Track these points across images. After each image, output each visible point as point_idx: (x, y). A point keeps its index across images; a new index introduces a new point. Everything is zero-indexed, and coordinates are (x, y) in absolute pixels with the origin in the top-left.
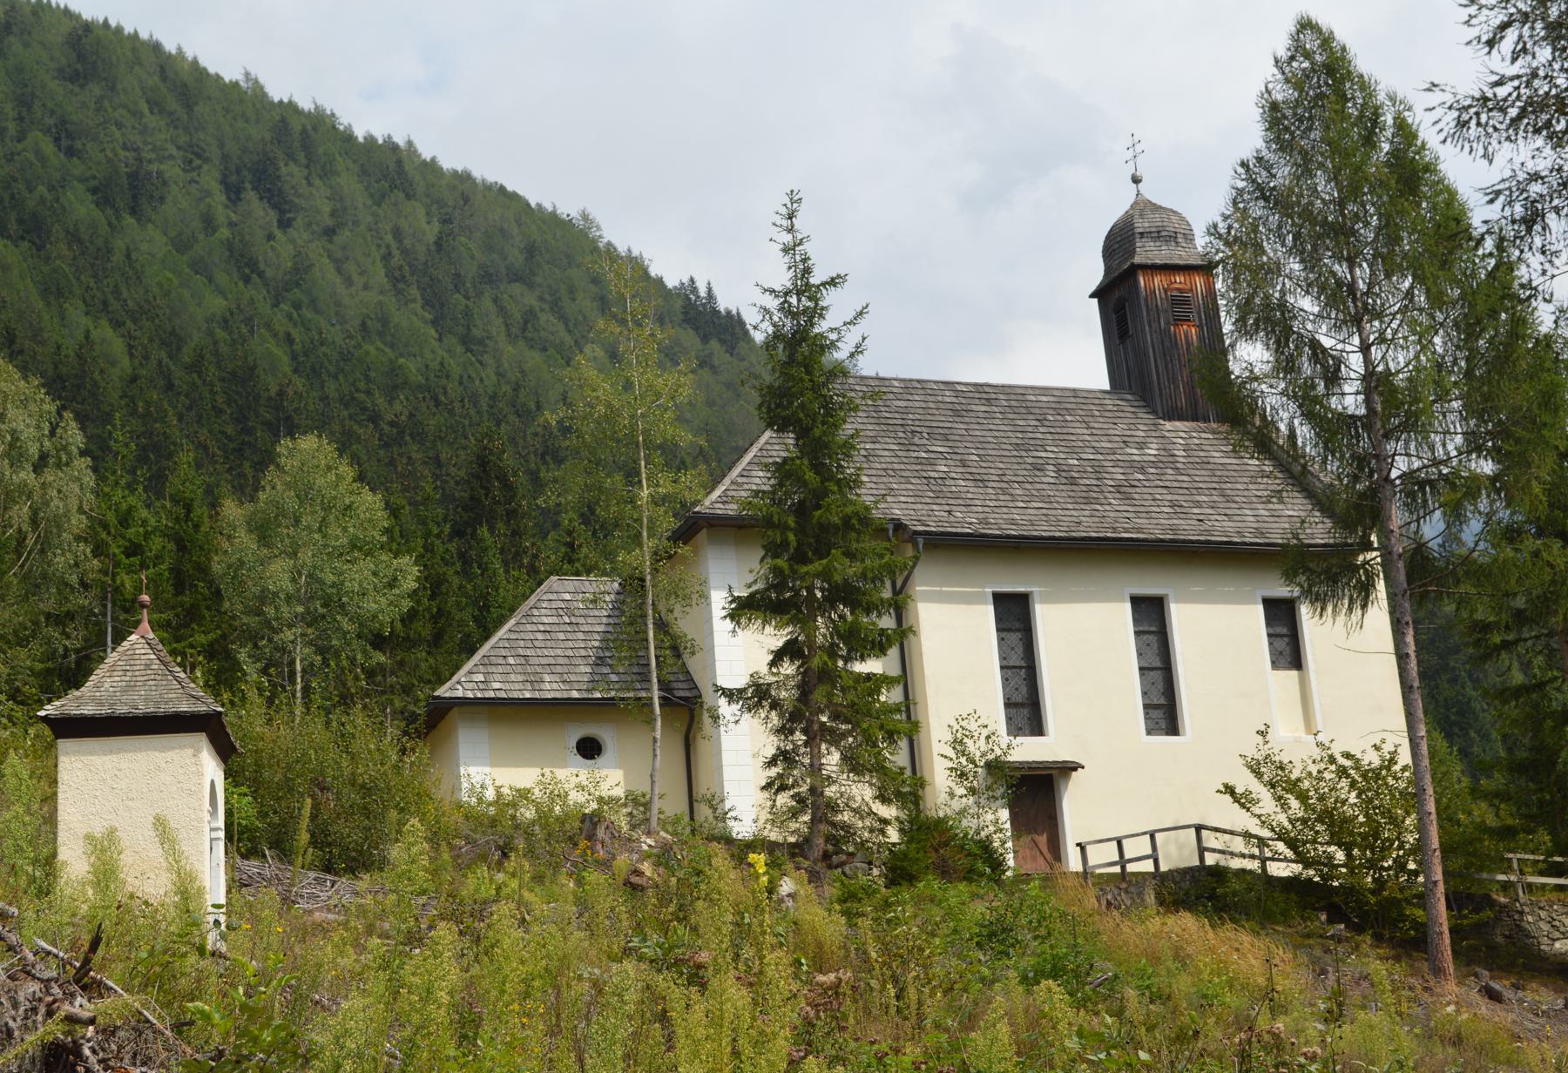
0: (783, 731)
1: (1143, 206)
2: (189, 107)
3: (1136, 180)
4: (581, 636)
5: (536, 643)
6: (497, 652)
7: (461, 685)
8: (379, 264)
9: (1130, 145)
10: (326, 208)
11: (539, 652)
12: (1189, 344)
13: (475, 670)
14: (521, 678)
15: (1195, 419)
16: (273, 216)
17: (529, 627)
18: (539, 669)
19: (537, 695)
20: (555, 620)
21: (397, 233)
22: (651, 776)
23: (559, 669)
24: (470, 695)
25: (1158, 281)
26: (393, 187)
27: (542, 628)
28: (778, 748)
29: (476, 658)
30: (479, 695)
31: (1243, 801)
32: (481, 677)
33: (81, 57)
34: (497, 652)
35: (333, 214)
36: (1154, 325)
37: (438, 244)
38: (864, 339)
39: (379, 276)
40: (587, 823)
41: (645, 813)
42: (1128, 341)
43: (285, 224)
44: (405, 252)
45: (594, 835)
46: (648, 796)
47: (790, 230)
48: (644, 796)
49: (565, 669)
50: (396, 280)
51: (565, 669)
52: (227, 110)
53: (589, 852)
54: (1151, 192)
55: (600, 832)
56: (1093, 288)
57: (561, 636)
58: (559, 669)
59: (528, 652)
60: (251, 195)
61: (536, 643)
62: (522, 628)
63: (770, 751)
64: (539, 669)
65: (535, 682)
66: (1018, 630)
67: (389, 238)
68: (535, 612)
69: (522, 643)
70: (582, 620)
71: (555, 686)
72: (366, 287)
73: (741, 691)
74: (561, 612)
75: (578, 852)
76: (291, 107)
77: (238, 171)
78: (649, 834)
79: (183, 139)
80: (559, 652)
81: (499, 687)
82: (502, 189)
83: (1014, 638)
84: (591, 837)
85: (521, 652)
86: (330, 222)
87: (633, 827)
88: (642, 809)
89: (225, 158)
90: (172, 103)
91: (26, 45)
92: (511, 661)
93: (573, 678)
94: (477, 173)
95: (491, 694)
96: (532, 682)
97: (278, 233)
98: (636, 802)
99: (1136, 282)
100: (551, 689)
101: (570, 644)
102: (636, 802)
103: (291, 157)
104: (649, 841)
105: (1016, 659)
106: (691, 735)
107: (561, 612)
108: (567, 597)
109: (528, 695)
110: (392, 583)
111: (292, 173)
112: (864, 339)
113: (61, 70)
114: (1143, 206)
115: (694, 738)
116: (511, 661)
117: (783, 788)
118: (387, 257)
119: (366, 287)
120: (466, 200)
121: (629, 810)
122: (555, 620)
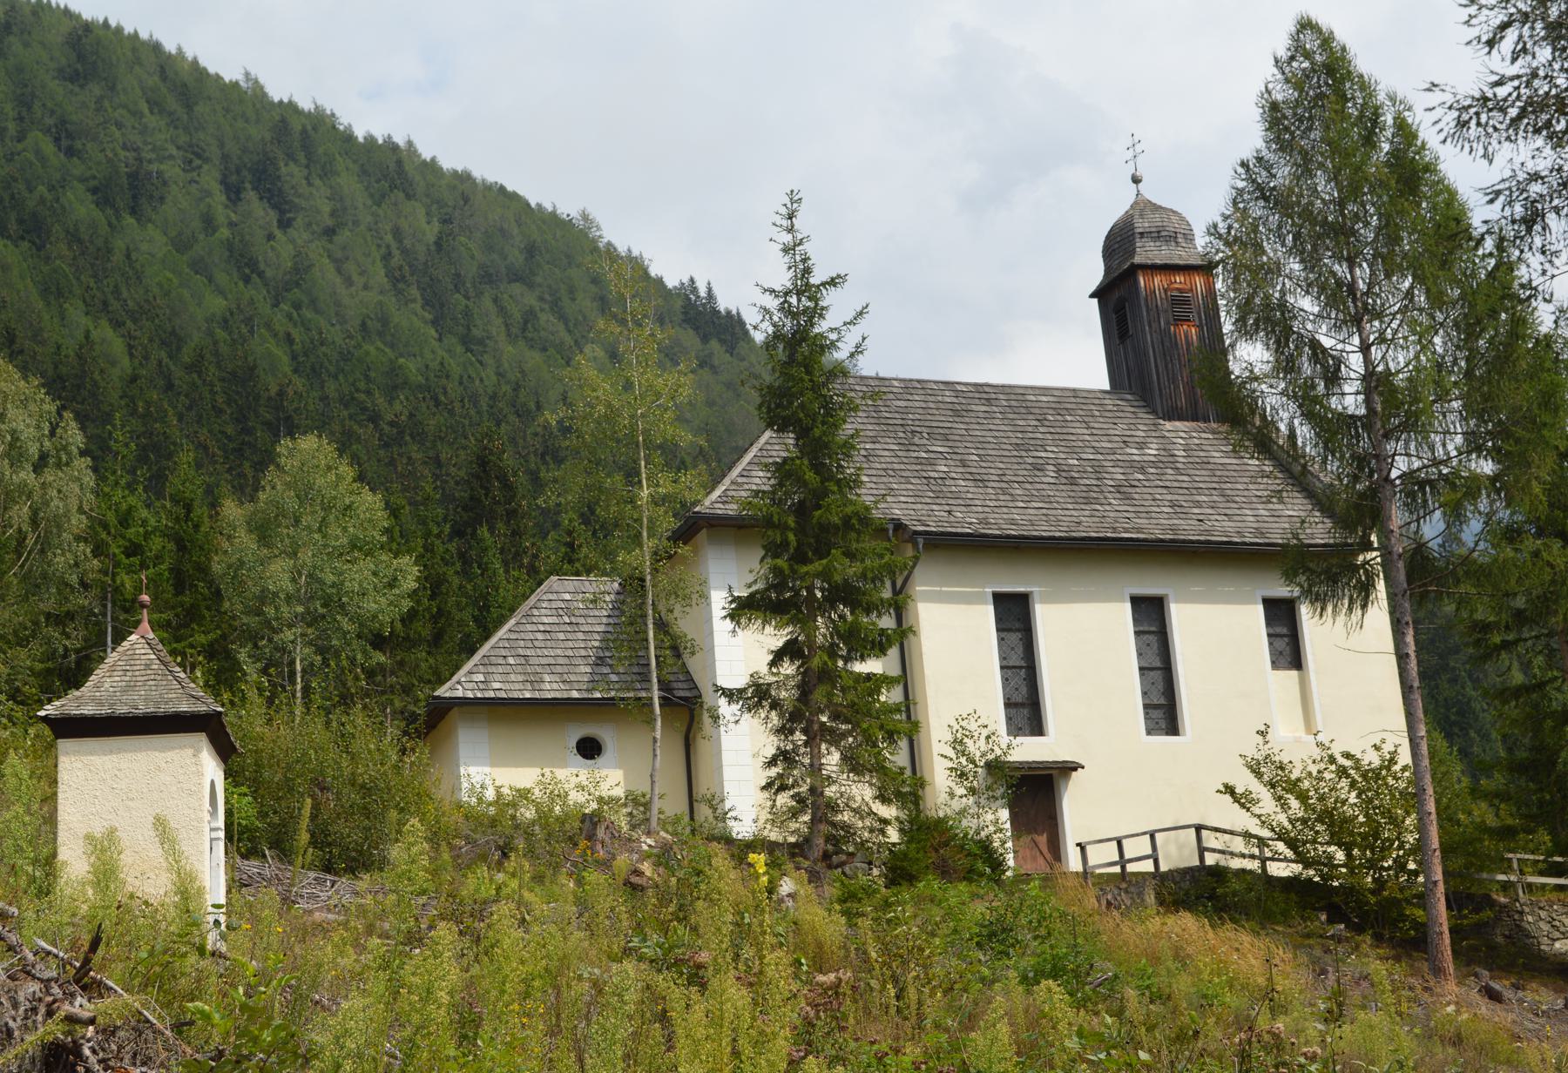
0: (783, 731)
1: (1143, 206)
2: (189, 107)
3: (1136, 180)
4: (581, 636)
5: (536, 643)
6: (497, 652)
7: (461, 685)
8: (379, 264)
9: (1130, 145)
10: (326, 208)
11: (539, 652)
12: (1189, 344)
13: (475, 670)
14: (521, 678)
15: (1195, 419)
16: (273, 216)
17: (529, 627)
18: (539, 669)
19: (537, 695)
20: (555, 620)
21: (397, 233)
22: (651, 776)
23: (559, 669)
24: (470, 695)
25: (1158, 281)
26: (393, 187)
27: (542, 628)
28: (778, 748)
29: (476, 658)
30: (479, 695)
31: (1243, 801)
32: (481, 677)
33: (81, 57)
34: (497, 652)
35: (333, 214)
36: (1154, 325)
37: (438, 244)
38: (864, 339)
39: (379, 276)
40: (587, 823)
41: (645, 813)
42: (1128, 341)
43: (285, 224)
44: (405, 252)
45: (594, 835)
46: (648, 796)
47: (790, 230)
48: (644, 796)
49: (565, 669)
50: (396, 280)
51: (565, 669)
52: (227, 110)
53: (589, 852)
54: (1151, 192)
55: (600, 832)
56: (1093, 288)
57: (561, 636)
58: (559, 669)
59: (528, 652)
60: (251, 195)
61: (536, 643)
62: (522, 628)
63: (770, 751)
64: (539, 669)
65: (535, 682)
66: (1018, 630)
67: (389, 238)
68: (535, 612)
69: (522, 643)
70: (582, 620)
71: (555, 686)
72: (366, 287)
73: (741, 691)
74: (561, 612)
75: (578, 852)
76: (291, 107)
77: (238, 171)
78: (649, 834)
79: (183, 139)
80: (559, 652)
81: (499, 687)
82: (502, 189)
83: (1014, 638)
84: (591, 837)
85: (521, 652)
86: (330, 222)
87: (633, 827)
88: (642, 809)
89: (225, 158)
90: (172, 103)
91: (26, 45)
92: (511, 661)
93: (573, 678)
94: (477, 173)
95: (491, 694)
96: (532, 682)
97: (278, 233)
98: (636, 802)
99: (1136, 282)
100: (551, 689)
101: (570, 644)
102: (636, 802)
103: (291, 157)
104: (649, 841)
105: (1016, 659)
106: (691, 735)
107: (561, 612)
108: (567, 597)
109: (528, 695)
110: (392, 583)
111: (292, 173)
112: (864, 339)
113: (61, 70)
114: (1143, 206)
115: (694, 738)
116: (511, 661)
117: (783, 788)
118: (387, 257)
119: (366, 287)
120: (466, 200)
121: (629, 810)
122: (555, 620)
